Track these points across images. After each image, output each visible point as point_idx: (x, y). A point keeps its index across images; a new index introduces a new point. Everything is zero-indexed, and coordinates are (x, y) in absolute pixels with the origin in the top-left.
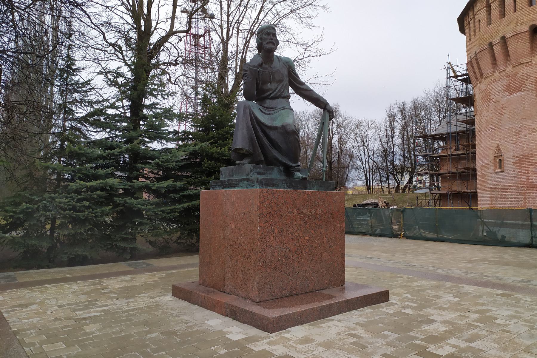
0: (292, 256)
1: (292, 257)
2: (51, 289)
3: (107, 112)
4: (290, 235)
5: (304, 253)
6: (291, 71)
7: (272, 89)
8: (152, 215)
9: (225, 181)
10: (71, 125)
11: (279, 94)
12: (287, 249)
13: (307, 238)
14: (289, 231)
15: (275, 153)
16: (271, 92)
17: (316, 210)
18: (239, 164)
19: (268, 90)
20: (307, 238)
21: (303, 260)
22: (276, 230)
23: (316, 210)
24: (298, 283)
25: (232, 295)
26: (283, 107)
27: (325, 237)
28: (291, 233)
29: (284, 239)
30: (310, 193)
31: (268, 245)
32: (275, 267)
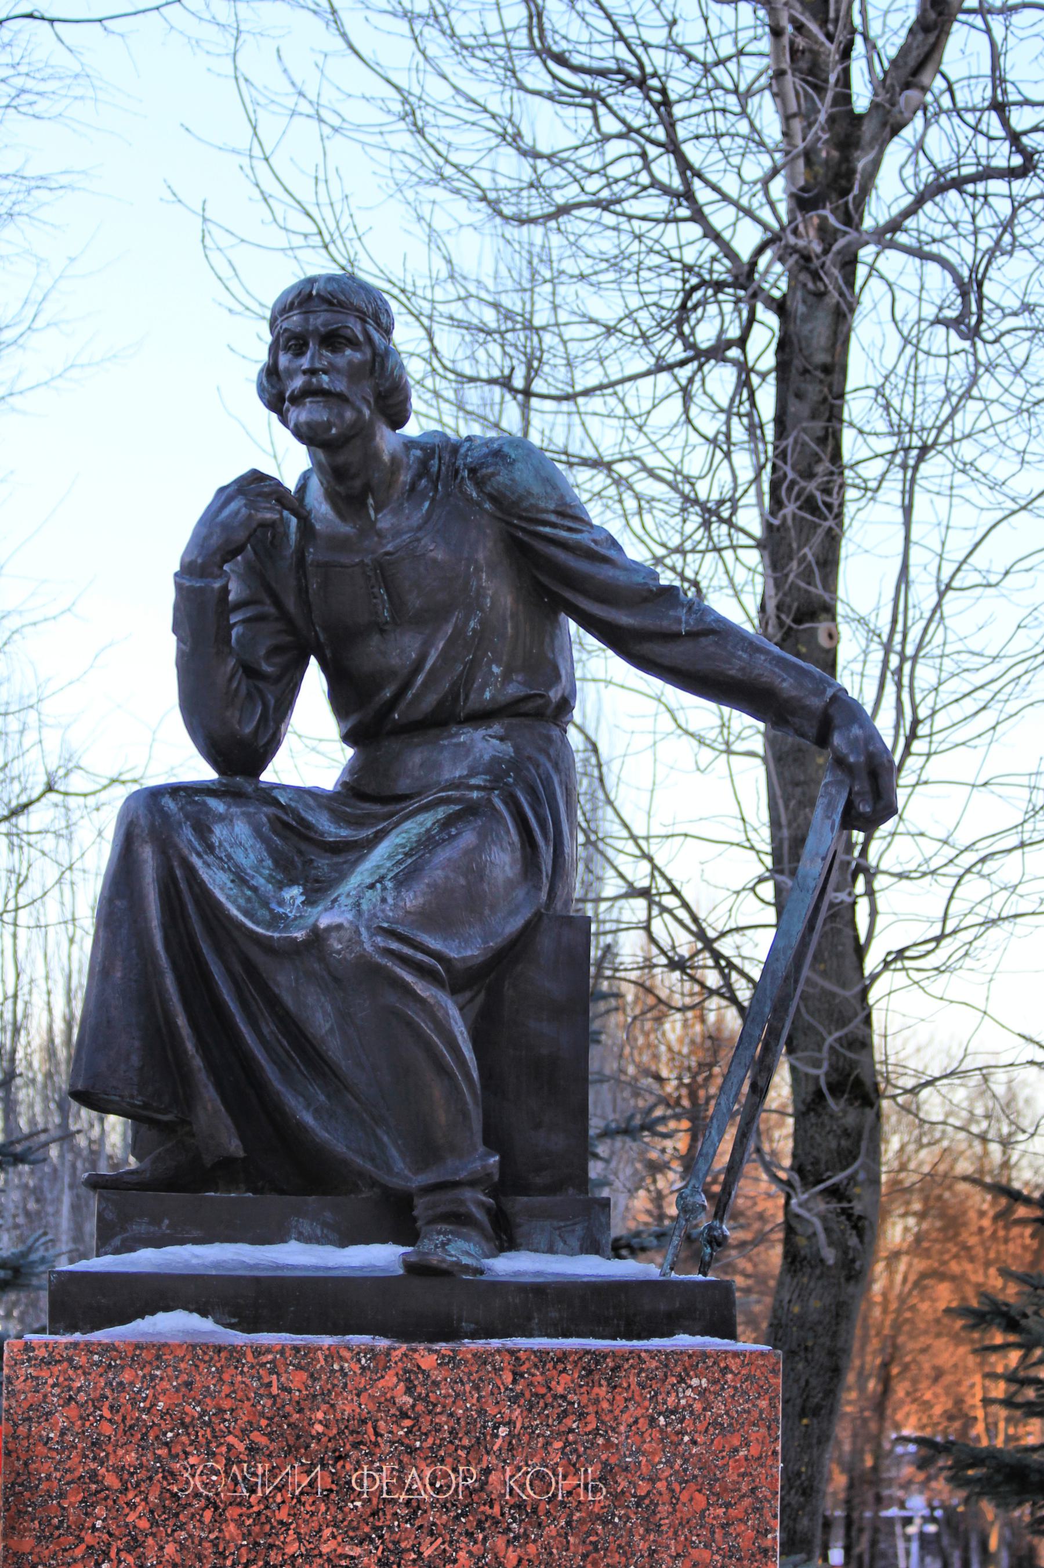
7: (393, 673)
11: (431, 700)
16: (388, 693)
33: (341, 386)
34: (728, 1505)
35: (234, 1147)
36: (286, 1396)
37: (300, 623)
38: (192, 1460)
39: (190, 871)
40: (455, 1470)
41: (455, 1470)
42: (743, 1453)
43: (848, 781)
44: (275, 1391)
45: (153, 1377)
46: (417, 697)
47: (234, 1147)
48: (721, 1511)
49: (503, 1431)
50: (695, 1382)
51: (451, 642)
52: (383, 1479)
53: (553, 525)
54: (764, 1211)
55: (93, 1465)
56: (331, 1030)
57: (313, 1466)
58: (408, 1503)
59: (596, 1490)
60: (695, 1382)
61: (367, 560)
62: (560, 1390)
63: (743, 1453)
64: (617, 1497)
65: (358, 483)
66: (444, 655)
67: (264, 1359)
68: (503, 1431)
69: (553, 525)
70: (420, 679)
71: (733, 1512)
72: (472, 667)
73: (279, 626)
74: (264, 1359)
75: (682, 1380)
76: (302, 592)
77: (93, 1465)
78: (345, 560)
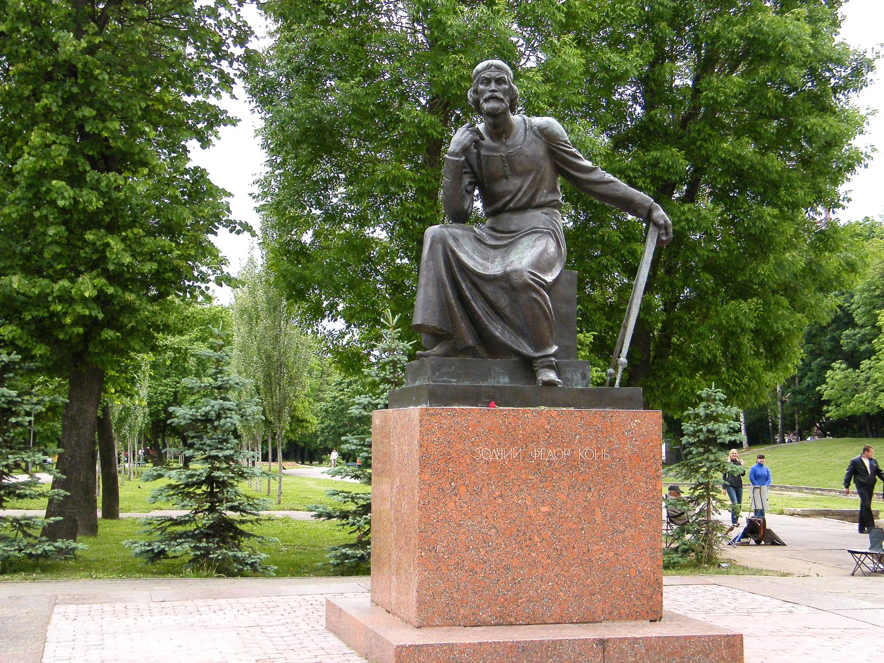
0: (505, 544)
1: (503, 546)
2: (683, 589)
3: (86, 237)
4: (500, 501)
5: (536, 539)
6: (554, 147)
7: (510, 192)
8: (356, 471)
9: (209, 358)
10: (193, 307)
11: (524, 200)
12: (491, 528)
13: (545, 509)
14: (497, 494)
15: (498, 330)
16: (508, 198)
17: (573, 450)
18: (422, 356)
19: (504, 194)
20: (545, 509)
21: (533, 555)
22: (463, 489)
23: (573, 450)
24: (520, 601)
25: (391, 615)
26: (534, 228)
27: (597, 509)
28: (501, 496)
29: (484, 508)
30: (554, 414)
31: (441, 517)
32: (458, 563)
33: (501, 96)
34: (647, 461)
35: (470, 342)
36: (510, 426)
37: (479, 175)
38: (480, 447)
39: (453, 252)
40: (563, 450)
41: (563, 450)
42: (651, 444)
43: (657, 230)
44: (507, 424)
45: (468, 420)
46: (520, 199)
47: (470, 342)
48: (644, 463)
49: (578, 437)
50: (636, 421)
51: (532, 182)
52: (541, 453)
53: (564, 146)
54: (400, 338)
55: (449, 450)
56: (507, 306)
57: (519, 449)
58: (549, 461)
59: (607, 456)
60: (636, 421)
61: (503, 155)
62: (595, 423)
63: (651, 444)
64: (613, 459)
65: (501, 130)
66: (530, 187)
67: (503, 413)
68: (578, 437)
69: (564, 146)
70: (520, 194)
71: (648, 463)
72: (537, 190)
73: (472, 175)
74: (503, 413)
75: (632, 420)
76: (479, 165)
77: (449, 450)
78: (495, 154)
